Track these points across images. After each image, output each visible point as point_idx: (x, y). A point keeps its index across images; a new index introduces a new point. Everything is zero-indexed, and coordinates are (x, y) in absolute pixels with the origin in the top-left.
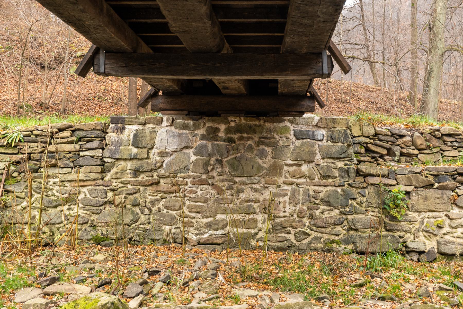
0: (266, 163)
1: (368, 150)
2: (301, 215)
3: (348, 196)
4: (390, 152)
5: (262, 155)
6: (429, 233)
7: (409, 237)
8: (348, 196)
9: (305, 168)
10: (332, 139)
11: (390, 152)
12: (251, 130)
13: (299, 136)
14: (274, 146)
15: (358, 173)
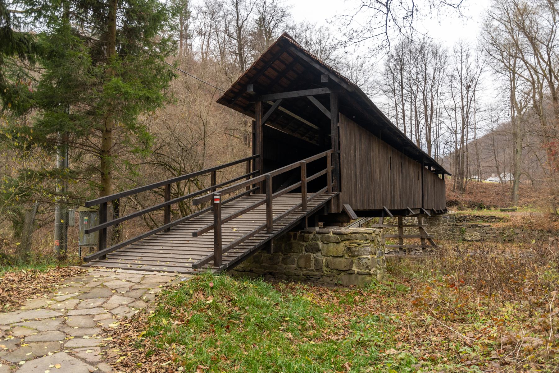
0: (437, 223)
1: (459, 220)
2: (444, 233)
3: (453, 229)
4: (464, 220)
5: (436, 221)
6: (470, 237)
7: (466, 237)
8: (453, 229)
9: (445, 224)
10: (450, 218)
11: (464, 220)
12: (434, 216)
13: (444, 218)
14: (439, 220)
15: (456, 225)
